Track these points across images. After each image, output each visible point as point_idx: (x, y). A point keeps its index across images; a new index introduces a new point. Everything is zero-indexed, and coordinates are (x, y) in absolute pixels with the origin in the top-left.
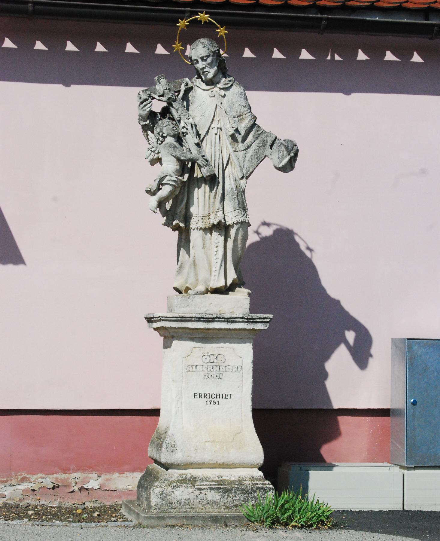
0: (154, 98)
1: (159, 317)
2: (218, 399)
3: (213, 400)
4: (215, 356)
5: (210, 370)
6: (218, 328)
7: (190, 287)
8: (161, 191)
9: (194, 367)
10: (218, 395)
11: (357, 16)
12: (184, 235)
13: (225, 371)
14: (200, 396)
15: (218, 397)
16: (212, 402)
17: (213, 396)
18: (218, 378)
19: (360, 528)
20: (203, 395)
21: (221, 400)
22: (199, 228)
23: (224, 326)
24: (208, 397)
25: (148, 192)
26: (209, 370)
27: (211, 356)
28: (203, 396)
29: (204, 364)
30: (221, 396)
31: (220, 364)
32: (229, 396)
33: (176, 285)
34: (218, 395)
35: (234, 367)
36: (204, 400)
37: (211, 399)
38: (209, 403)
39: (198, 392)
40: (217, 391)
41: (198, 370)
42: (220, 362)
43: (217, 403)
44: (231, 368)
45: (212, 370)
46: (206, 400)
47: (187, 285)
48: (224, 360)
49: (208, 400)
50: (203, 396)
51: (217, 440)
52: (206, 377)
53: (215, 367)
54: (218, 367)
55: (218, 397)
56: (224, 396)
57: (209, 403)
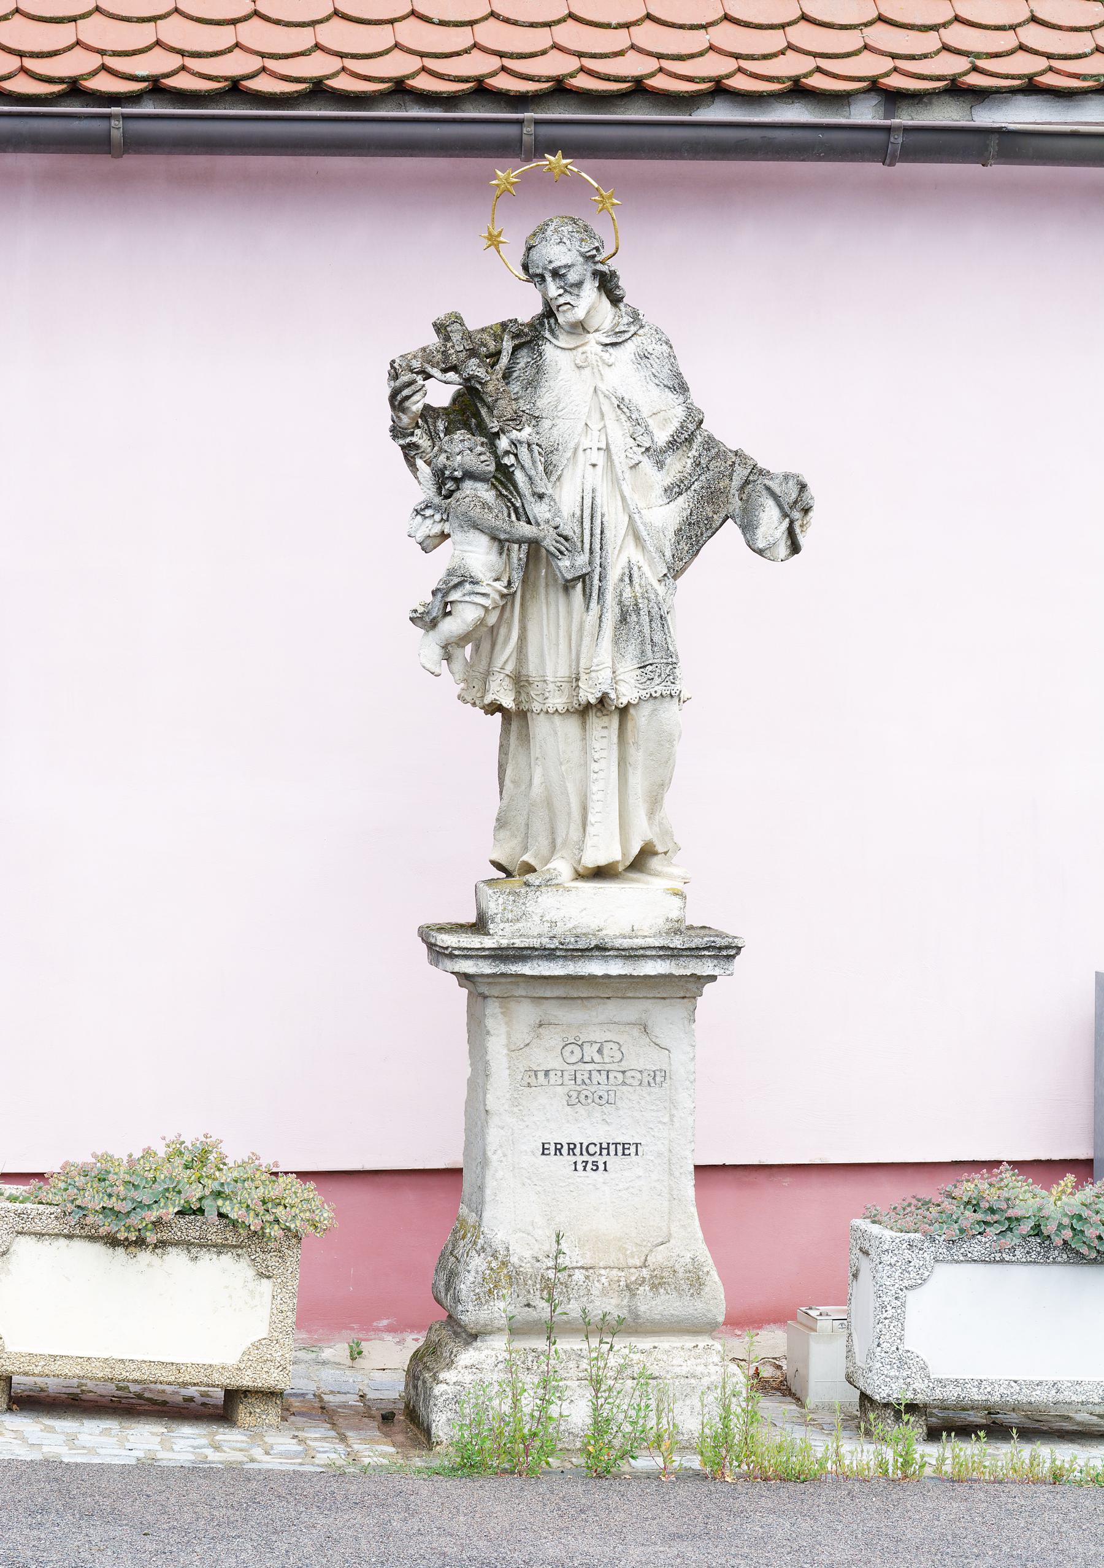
0: (428, 376)
1: (447, 948)
2: (605, 1158)
3: (591, 1159)
4: (596, 1047)
5: (584, 1082)
6: (600, 974)
7: (533, 862)
8: (449, 618)
9: (541, 1075)
10: (605, 1146)
11: (623, 113)
12: (514, 726)
13: (624, 1083)
14: (558, 1150)
15: (605, 1152)
16: (590, 1166)
17: (592, 1149)
18: (603, 1102)
19: (968, 21)
20: (566, 1147)
21: (612, 1160)
22: (551, 710)
23: (616, 968)
24: (577, 1151)
25: (417, 619)
26: (579, 1081)
27: (586, 1047)
28: (565, 1151)
29: (567, 1067)
30: (612, 1148)
31: (608, 1067)
32: (633, 1149)
33: (495, 857)
34: (605, 1146)
35: (645, 1074)
36: (567, 1160)
37: (586, 1157)
38: (580, 1167)
39: (552, 1138)
40: (600, 1134)
41: (552, 1082)
42: (607, 1060)
43: (602, 1167)
44: (638, 1075)
45: (587, 1081)
46: (573, 1159)
47: (526, 858)
48: (618, 1056)
49: (580, 1159)
50: (565, 1151)
51: (601, 1264)
52: (574, 1100)
53: (595, 1074)
54: (604, 1073)
55: (605, 1152)
56: (620, 1148)
57: (580, 1167)
